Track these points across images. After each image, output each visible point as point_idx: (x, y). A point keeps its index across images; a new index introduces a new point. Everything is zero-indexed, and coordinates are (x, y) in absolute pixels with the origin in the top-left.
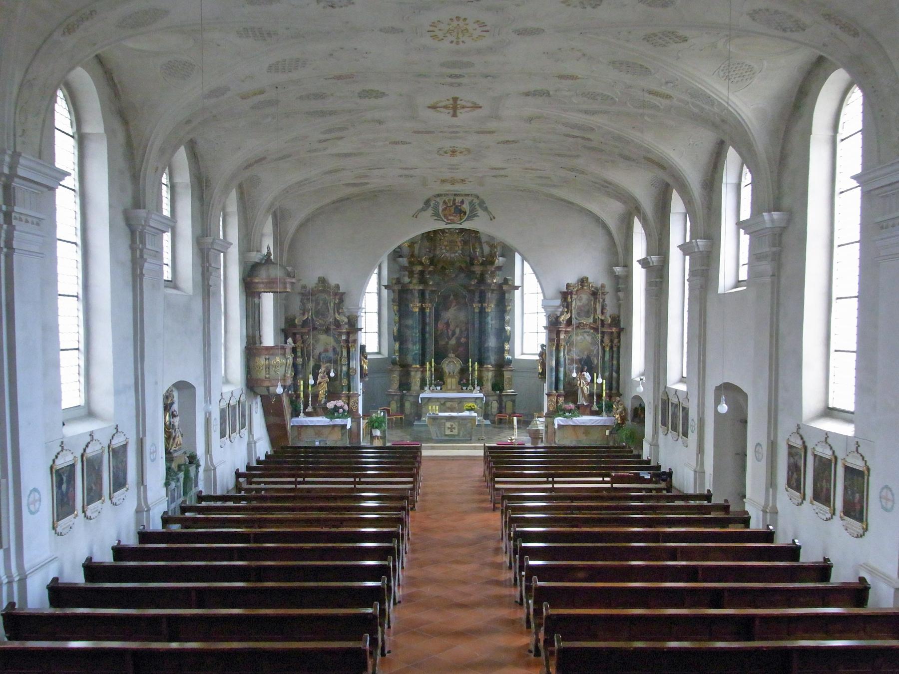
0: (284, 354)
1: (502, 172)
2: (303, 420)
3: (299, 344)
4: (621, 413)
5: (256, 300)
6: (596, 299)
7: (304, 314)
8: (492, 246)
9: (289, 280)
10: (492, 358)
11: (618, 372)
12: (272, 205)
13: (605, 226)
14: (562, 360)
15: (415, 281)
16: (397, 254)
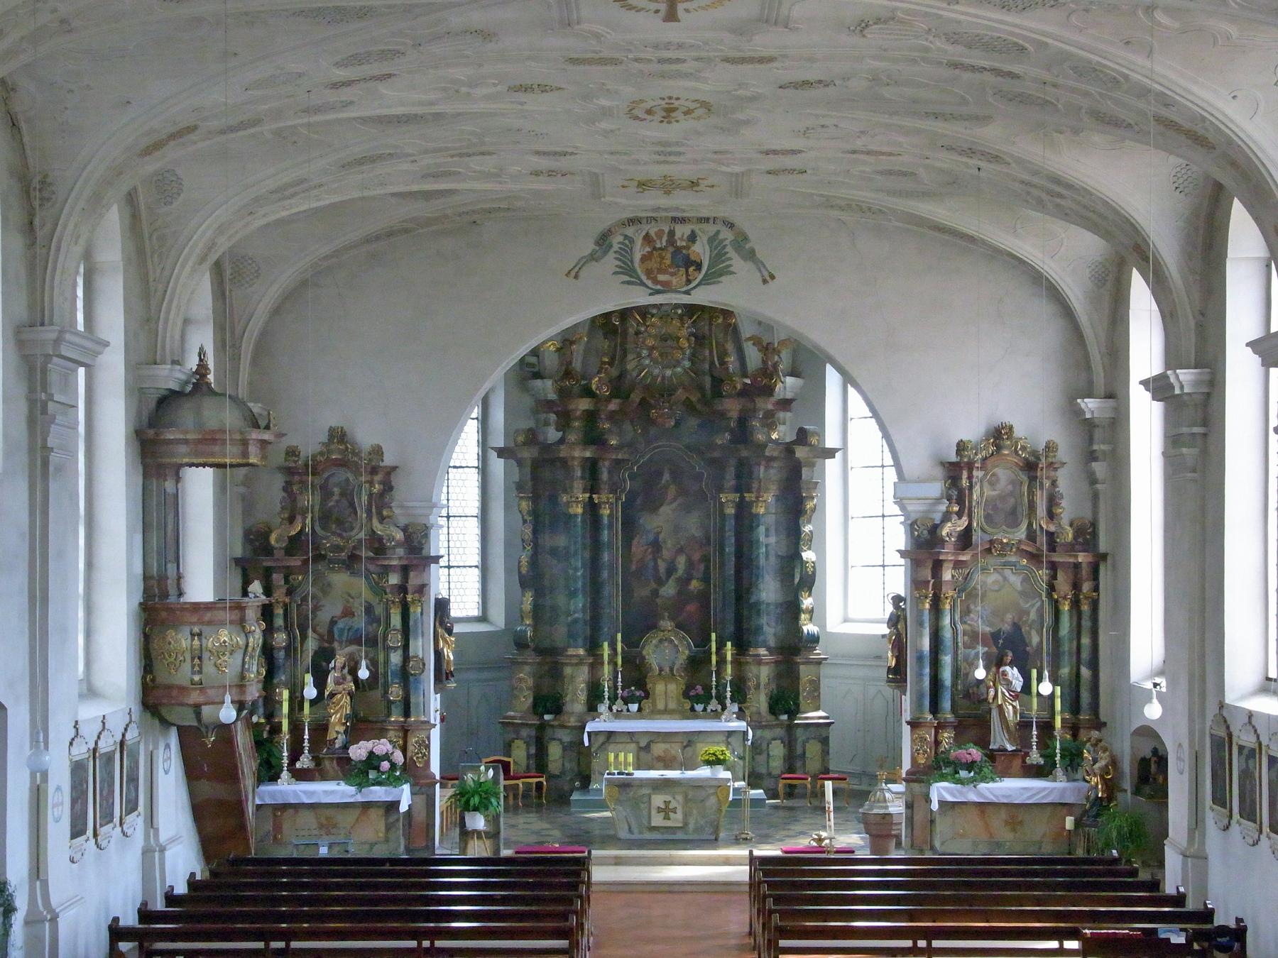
0: (241, 622)
1: (789, 162)
2: (287, 789)
3: (279, 595)
4: (1105, 770)
5: (169, 485)
6: (1033, 479)
7: (291, 520)
8: (767, 349)
9: (255, 435)
10: (770, 630)
11: (1094, 665)
12: (211, 246)
13: (1054, 294)
14: (947, 634)
15: (572, 437)
16: (529, 370)
